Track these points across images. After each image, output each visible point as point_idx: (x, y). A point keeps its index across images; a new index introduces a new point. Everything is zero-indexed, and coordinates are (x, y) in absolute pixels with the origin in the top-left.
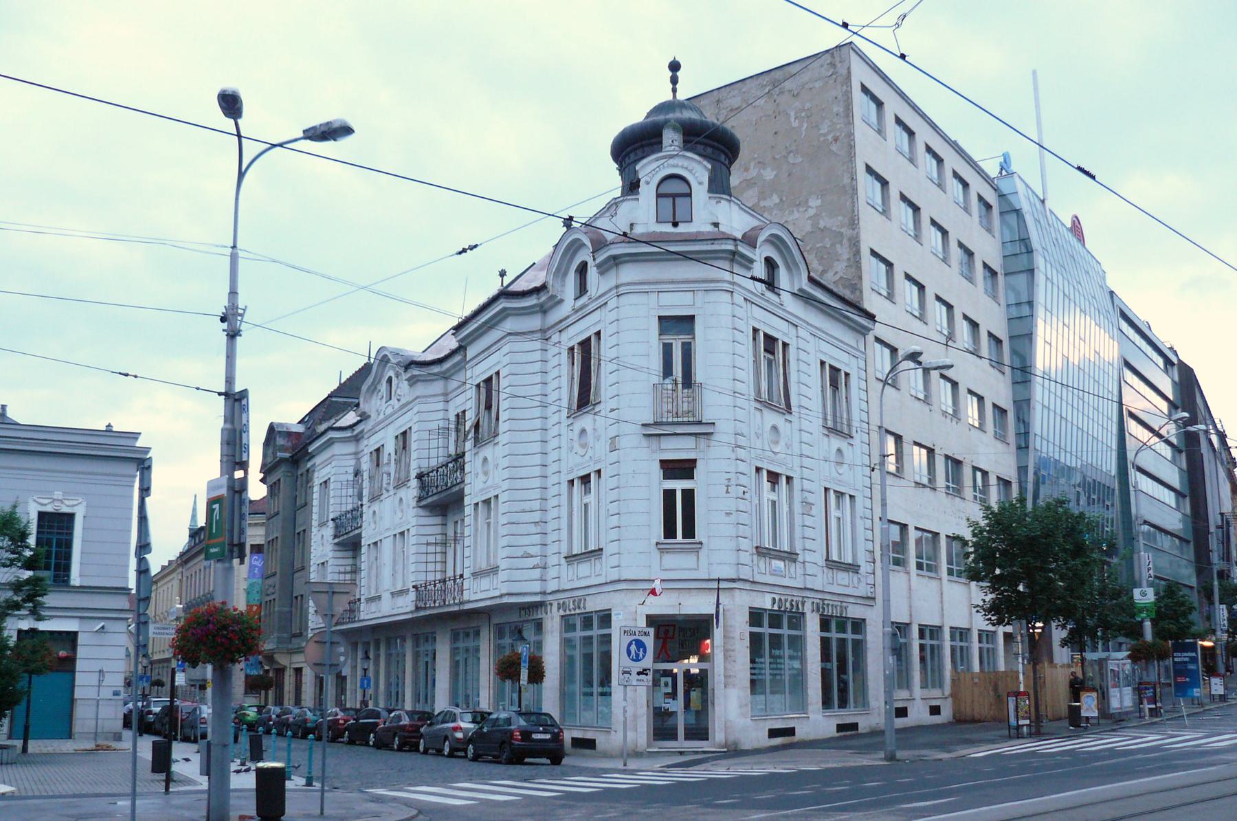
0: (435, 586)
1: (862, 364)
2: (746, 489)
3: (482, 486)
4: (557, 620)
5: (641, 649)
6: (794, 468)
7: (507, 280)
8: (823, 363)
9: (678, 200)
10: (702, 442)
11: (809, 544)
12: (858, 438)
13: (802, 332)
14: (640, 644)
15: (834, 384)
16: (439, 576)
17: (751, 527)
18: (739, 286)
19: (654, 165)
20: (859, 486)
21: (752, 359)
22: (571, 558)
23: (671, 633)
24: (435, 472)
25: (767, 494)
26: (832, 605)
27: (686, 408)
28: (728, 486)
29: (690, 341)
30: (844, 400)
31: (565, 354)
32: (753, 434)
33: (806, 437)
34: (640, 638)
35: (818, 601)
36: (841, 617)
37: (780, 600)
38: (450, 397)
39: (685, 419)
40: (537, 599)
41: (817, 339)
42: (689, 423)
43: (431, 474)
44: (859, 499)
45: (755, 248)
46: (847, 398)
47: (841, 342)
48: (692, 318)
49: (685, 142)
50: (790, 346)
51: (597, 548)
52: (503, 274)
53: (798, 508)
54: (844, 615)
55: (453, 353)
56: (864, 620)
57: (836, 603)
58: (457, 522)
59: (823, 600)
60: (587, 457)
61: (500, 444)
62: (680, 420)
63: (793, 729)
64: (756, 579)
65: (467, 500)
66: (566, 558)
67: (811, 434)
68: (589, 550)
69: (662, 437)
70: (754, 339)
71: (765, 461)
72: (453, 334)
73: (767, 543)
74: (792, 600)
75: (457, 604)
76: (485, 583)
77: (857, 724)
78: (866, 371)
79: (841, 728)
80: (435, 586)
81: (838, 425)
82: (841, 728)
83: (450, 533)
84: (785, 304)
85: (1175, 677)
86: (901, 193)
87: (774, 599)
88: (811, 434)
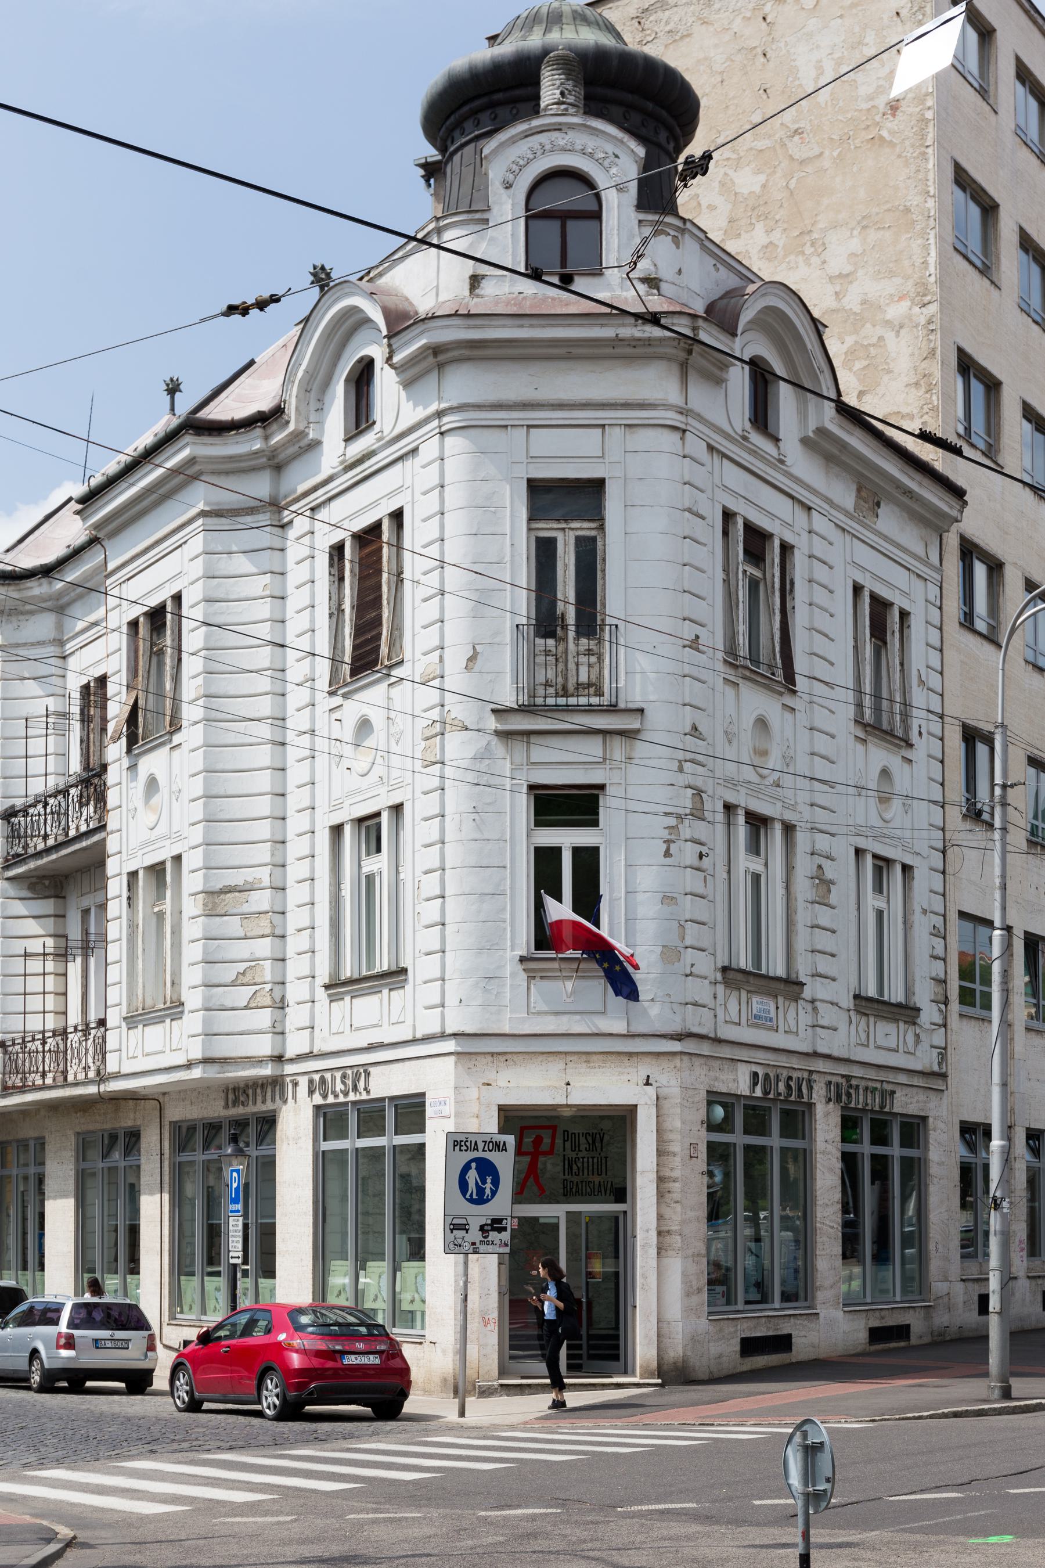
0: (44, 1043)
1: (933, 591)
2: (705, 850)
3: (145, 835)
4: (306, 1116)
5: (489, 1179)
6: (799, 808)
7: (185, 404)
8: (857, 589)
9: (571, 225)
10: (618, 748)
11: (824, 965)
12: (923, 747)
13: (819, 523)
14: (487, 1169)
15: (879, 630)
16: (51, 1023)
17: (713, 928)
18: (700, 418)
19: (523, 148)
20: (922, 847)
21: (720, 575)
22: (337, 986)
23: (547, 1141)
24: (40, 807)
25: (745, 863)
26: (867, 1088)
27: (583, 678)
28: (668, 842)
29: (593, 533)
30: (898, 668)
31: (323, 561)
32: (720, 735)
33: (822, 744)
34: (487, 1155)
35: (840, 1080)
36: (881, 1112)
37: (767, 1076)
38: (69, 647)
39: (583, 701)
40: (267, 1071)
41: (848, 538)
42: (590, 709)
43: (31, 811)
44: (920, 874)
45: (734, 335)
46: (902, 664)
47: (898, 546)
48: (599, 485)
49: (588, 98)
50: (796, 551)
51: (394, 968)
52: (173, 389)
53: (803, 888)
54: (887, 1109)
55: (75, 554)
56: (924, 1119)
57: (874, 1085)
58: (86, 912)
59: (848, 1078)
60: (373, 777)
61: (185, 747)
62: (572, 701)
63: (788, 1337)
64: (721, 1035)
65: (112, 866)
66: (327, 987)
67: (833, 737)
68: (377, 970)
69: (533, 739)
70: (726, 533)
71: (743, 791)
72: (78, 513)
73: (744, 961)
74: (790, 1078)
75: (92, 1082)
76: (154, 1035)
77: (908, 1326)
78: (940, 608)
79: (750, 1346)
80: (44, 1043)
81: (885, 717)
82: (877, 1335)
83: (75, 933)
84: (789, 461)
85: (588, 1350)
86: (1021, 229)
87: (755, 1075)
88: (833, 737)
